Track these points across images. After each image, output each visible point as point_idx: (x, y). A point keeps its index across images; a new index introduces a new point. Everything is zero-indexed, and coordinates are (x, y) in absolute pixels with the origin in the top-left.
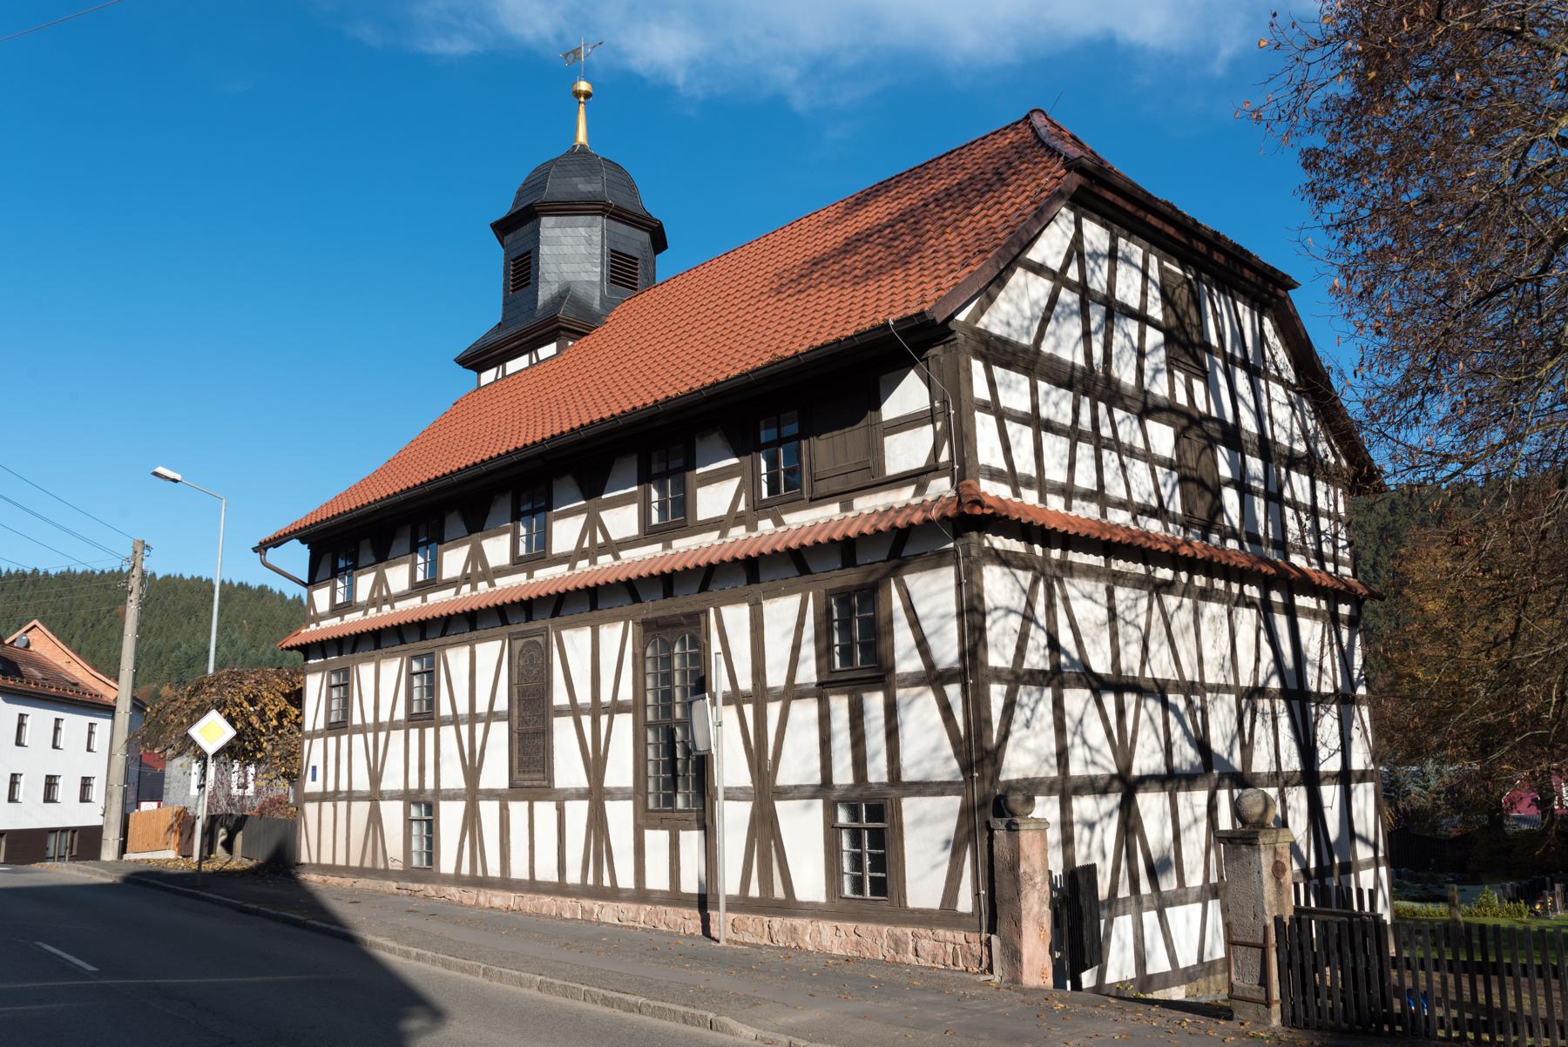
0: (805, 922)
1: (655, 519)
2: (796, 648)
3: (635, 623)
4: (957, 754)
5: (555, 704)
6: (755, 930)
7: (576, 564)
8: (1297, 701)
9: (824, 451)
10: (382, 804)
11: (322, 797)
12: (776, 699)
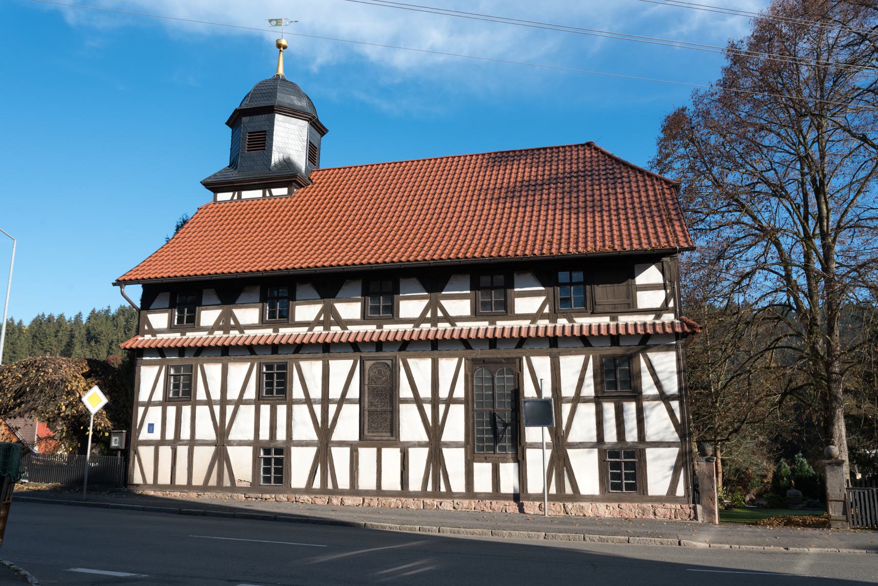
2: (581, 380)
3: (466, 359)
4: (677, 431)
6: (553, 510)
9: (602, 292)
12: (568, 402)
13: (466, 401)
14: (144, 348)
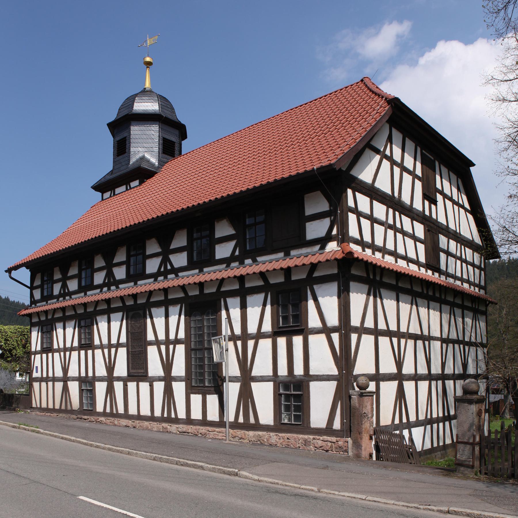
0: (264, 433)
1: (195, 259)
5: (148, 340)
7: (230, 264)
8: (462, 345)
10: (69, 382)
11: (41, 380)
12: (252, 338)
13: (127, 345)
14: (137, 293)
